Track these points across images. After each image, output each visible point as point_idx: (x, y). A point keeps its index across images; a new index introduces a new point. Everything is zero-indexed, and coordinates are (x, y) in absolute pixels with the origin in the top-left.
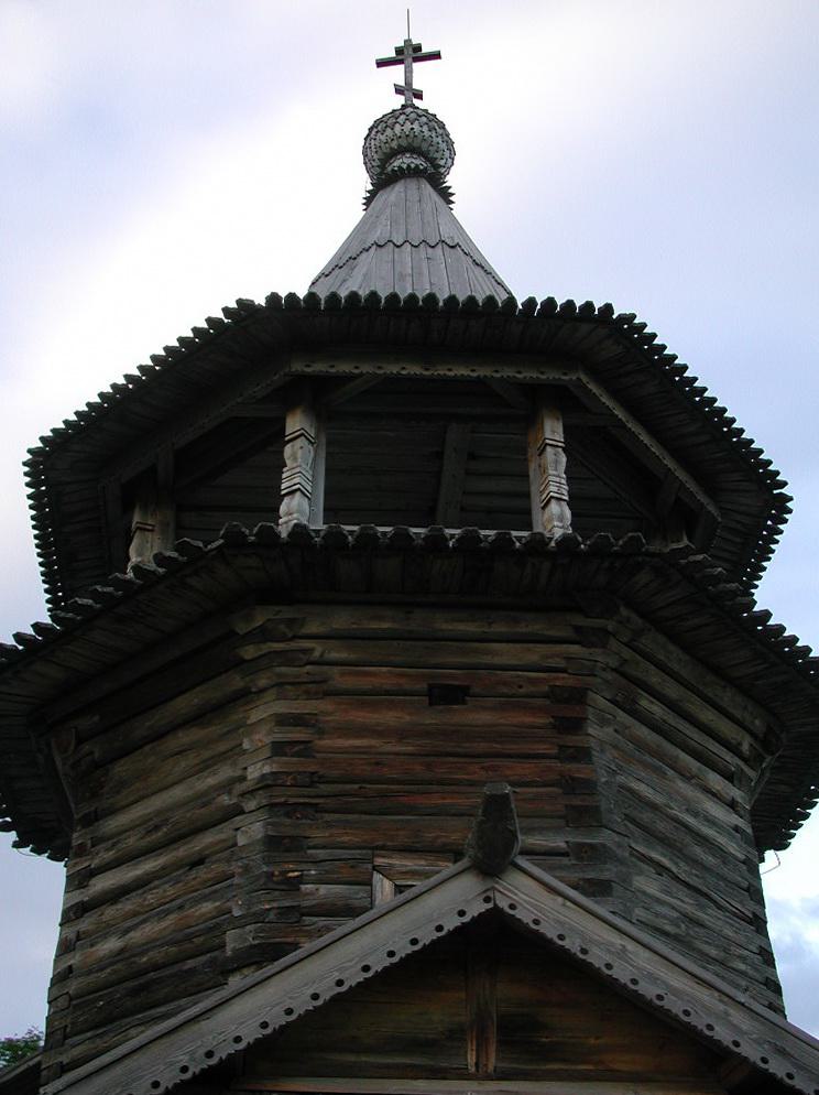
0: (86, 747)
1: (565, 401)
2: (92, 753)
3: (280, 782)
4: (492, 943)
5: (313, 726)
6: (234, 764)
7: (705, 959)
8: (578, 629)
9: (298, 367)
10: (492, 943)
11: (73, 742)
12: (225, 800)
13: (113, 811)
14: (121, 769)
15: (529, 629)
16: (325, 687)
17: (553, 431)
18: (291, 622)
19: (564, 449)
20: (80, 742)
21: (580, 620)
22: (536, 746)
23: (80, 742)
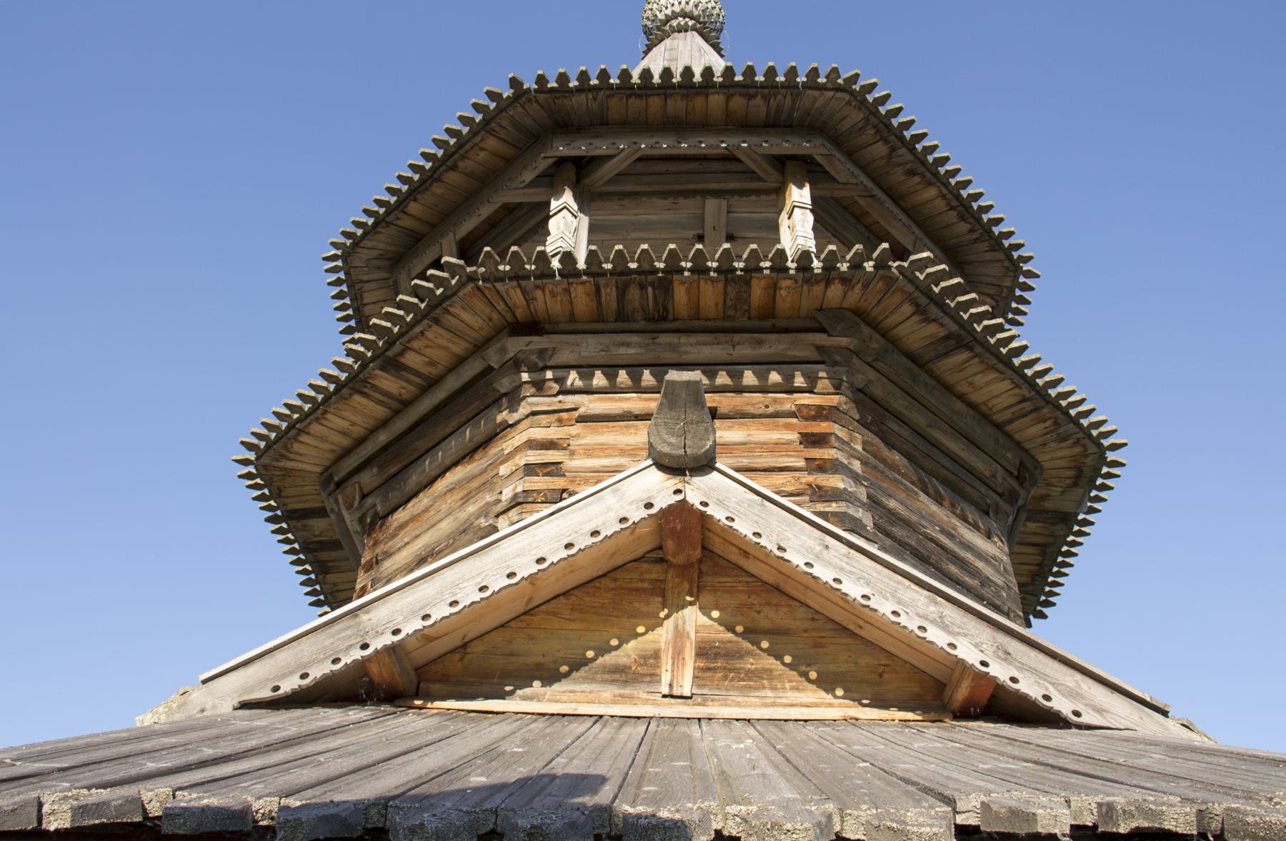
0: (370, 501)
1: (808, 170)
2: (375, 505)
3: (530, 499)
4: (682, 523)
5: (565, 449)
6: (492, 490)
7: (967, 590)
8: (820, 349)
9: (562, 150)
10: (682, 523)
11: (357, 497)
12: (483, 522)
13: (388, 555)
14: (401, 516)
15: (772, 350)
16: (576, 414)
17: (800, 195)
18: (541, 353)
19: (812, 211)
20: (364, 496)
21: (820, 338)
22: (781, 459)
23: (364, 496)
